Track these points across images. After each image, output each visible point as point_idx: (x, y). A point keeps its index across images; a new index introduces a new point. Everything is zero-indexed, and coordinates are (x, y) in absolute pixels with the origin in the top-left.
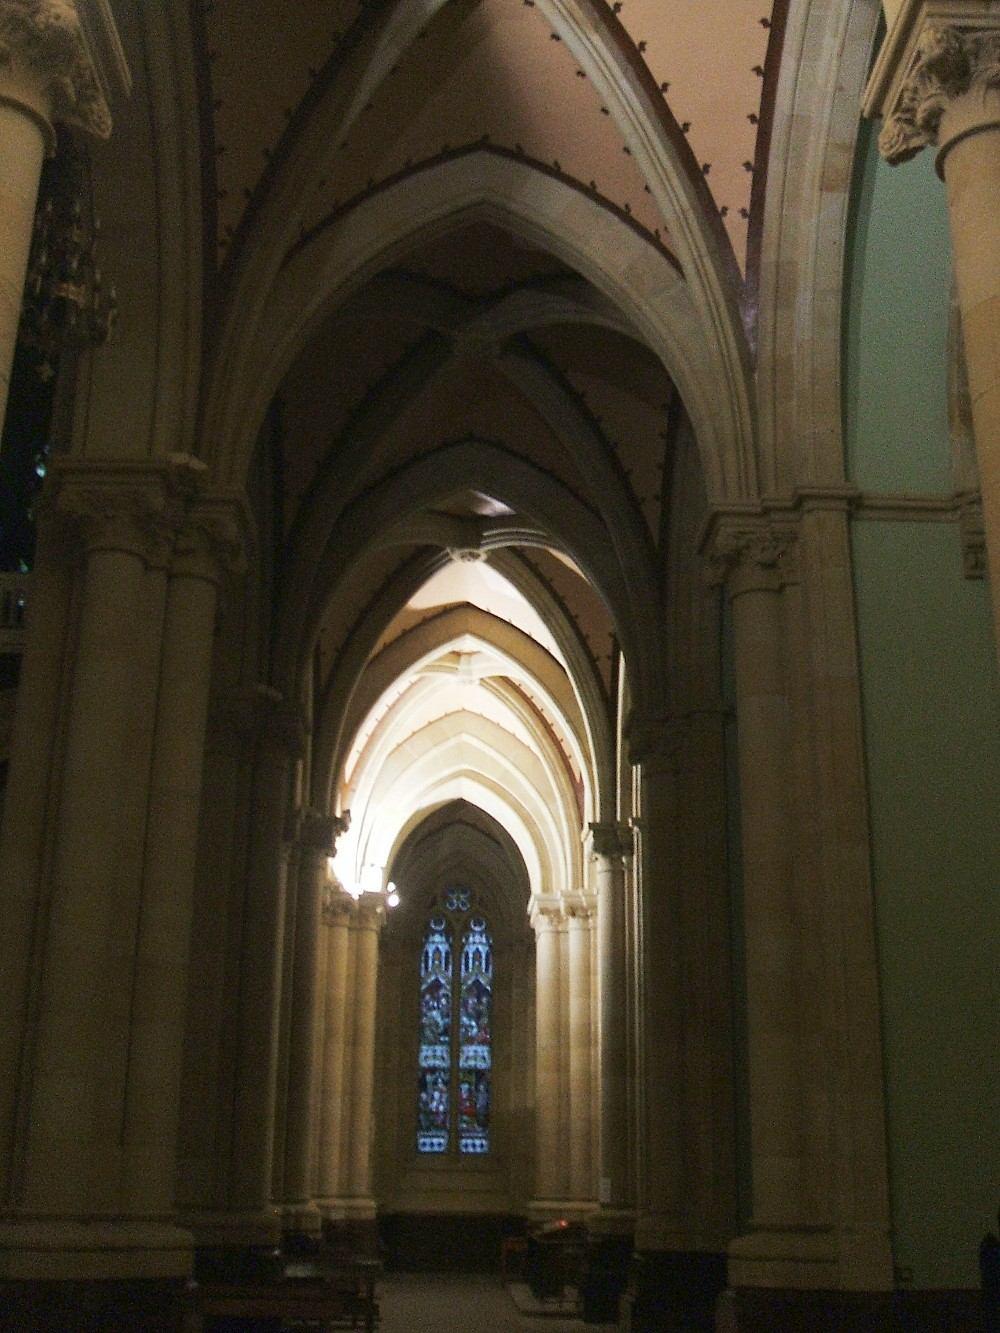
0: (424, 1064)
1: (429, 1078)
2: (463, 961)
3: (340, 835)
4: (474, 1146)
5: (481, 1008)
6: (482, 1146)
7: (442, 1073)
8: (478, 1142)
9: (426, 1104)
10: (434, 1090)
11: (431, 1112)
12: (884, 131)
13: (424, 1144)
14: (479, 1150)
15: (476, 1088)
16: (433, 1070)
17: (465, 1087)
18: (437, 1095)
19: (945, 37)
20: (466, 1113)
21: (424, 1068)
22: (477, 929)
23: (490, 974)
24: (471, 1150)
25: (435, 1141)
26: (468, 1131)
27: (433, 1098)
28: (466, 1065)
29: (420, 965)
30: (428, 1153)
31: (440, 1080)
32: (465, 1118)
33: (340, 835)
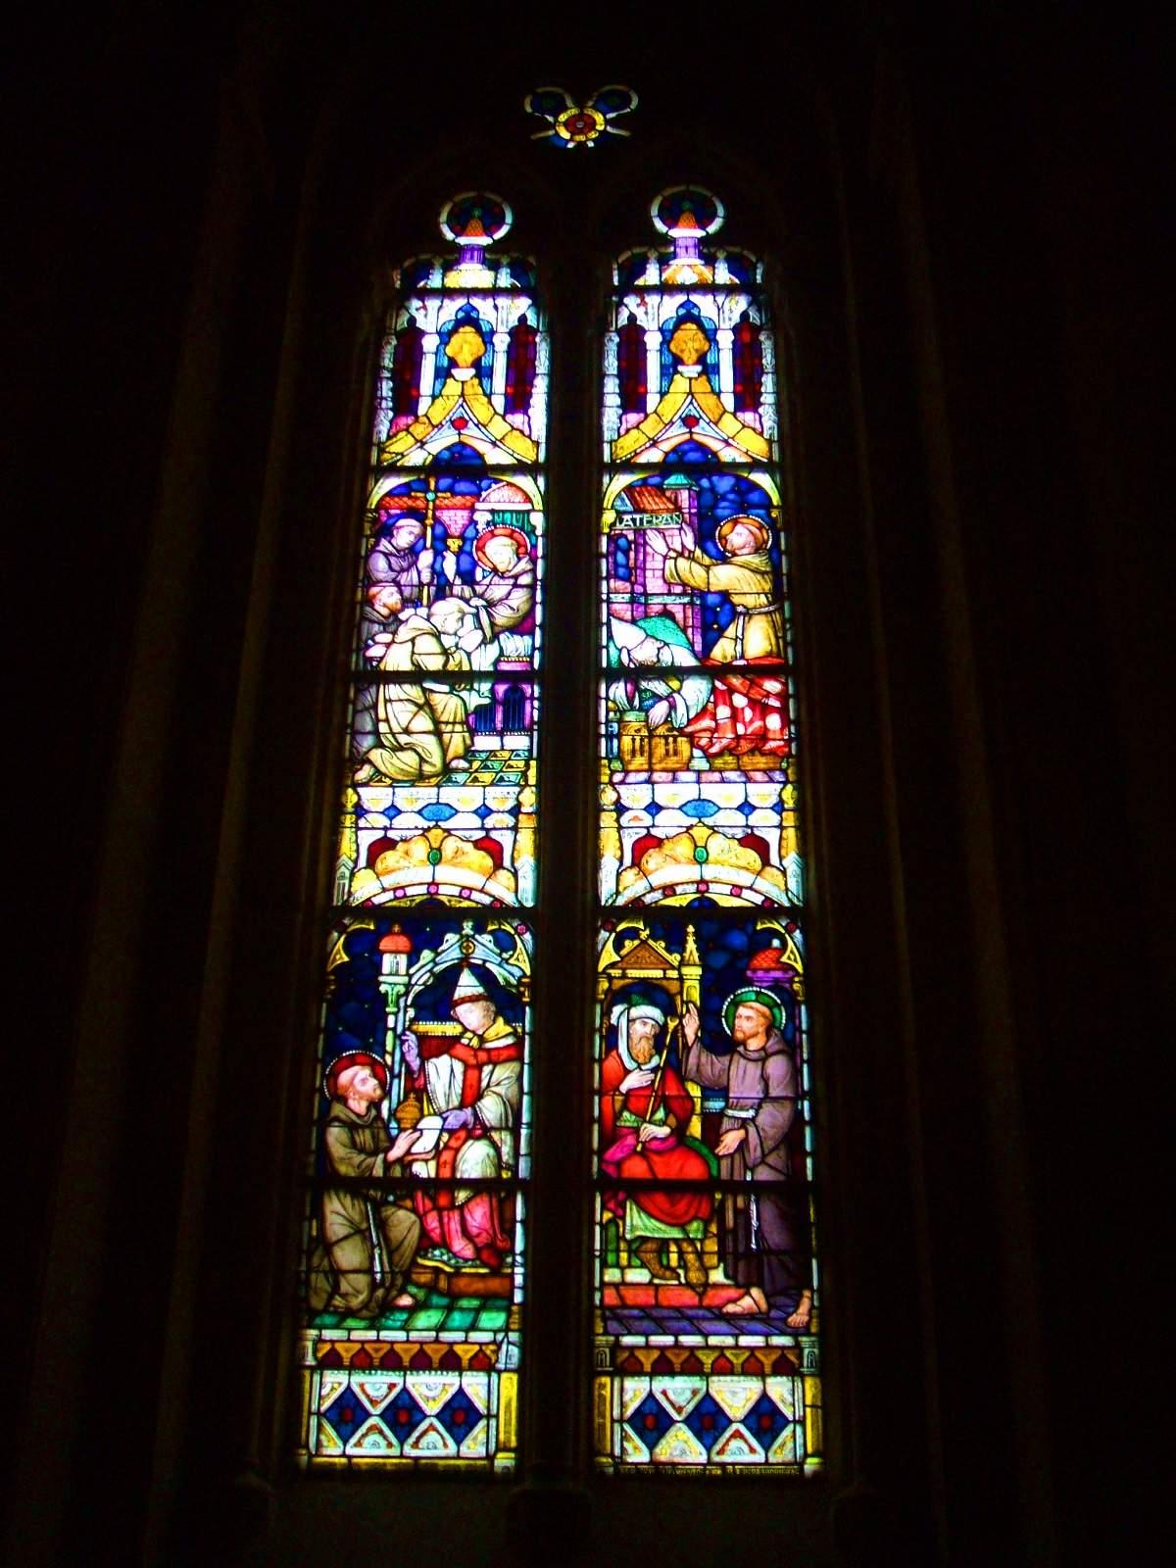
0: (365, 887)
1: (398, 972)
2: (611, 364)
3: (424, 1372)
4: (708, 1420)
5: (723, 577)
6: (765, 1420)
7: (484, 949)
8: (736, 1395)
9: (376, 1130)
10: (431, 1047)
11: (403, 1185)
12: (460, 1234)
13: (348, 1414)
14: (740, 1451)
15: (709, 1013)
16: (426, 920)
17: (639, 1022)
18: (443, 1075)
19: (451, 1255)
20: (641, 1191)
21: (368, 909)
22: (686, 233)
23: (768, 413)
24: (681, 1447)
25: (431, 1389)
26: (655, 1317)
27: (417, 1088)
28: (634, 887)
29: (375, 387)
30: (377, 1475)
31: (468, 984)
32: (638, 1223)
33: (424, 1372)
